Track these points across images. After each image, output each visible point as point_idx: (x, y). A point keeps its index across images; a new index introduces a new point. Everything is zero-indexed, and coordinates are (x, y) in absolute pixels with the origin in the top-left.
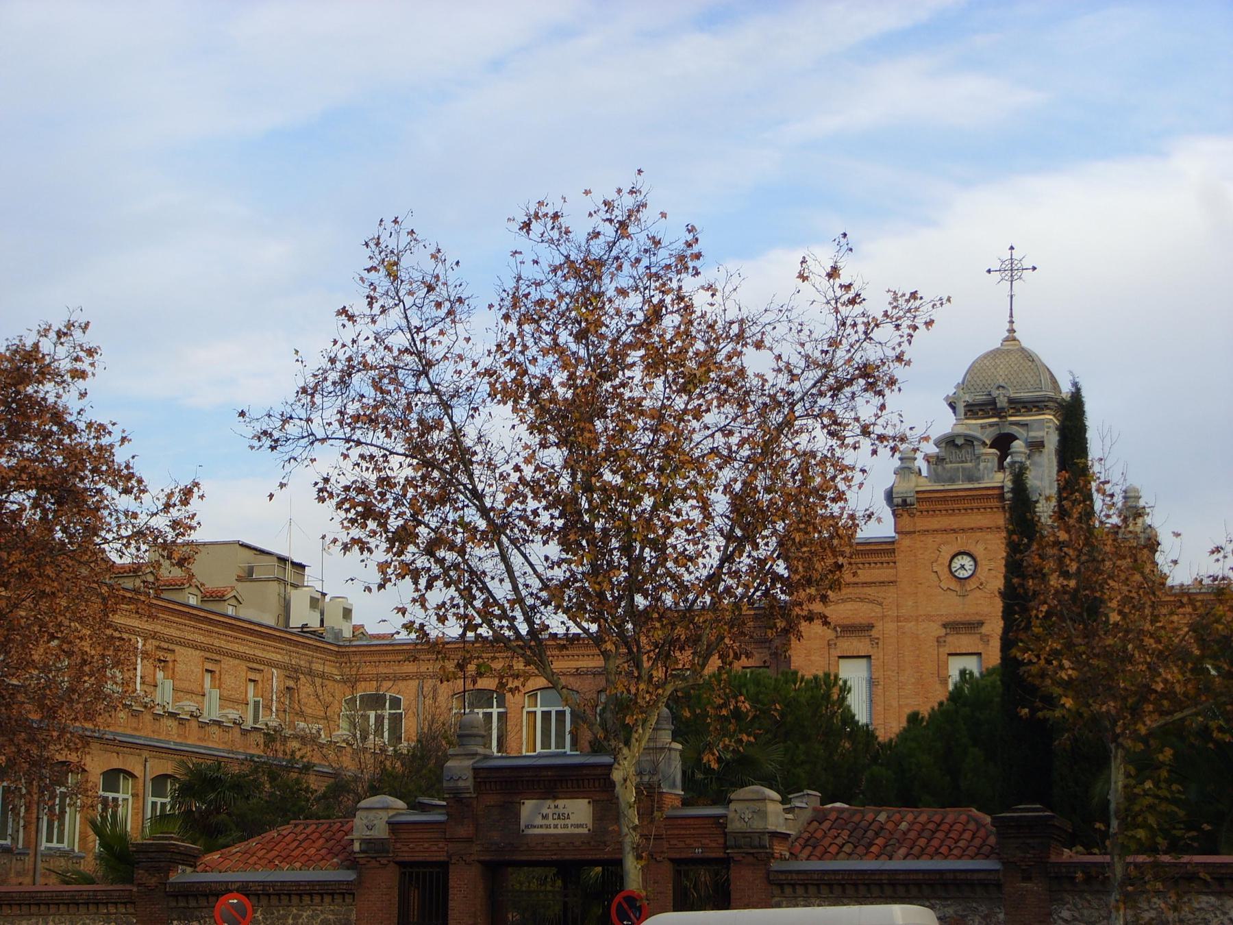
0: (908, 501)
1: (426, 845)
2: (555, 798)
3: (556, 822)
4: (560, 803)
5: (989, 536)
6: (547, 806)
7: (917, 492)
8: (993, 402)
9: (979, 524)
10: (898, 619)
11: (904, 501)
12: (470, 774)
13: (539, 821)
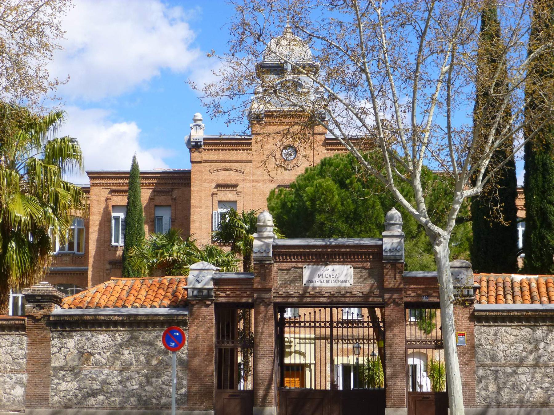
3: (328, 279)
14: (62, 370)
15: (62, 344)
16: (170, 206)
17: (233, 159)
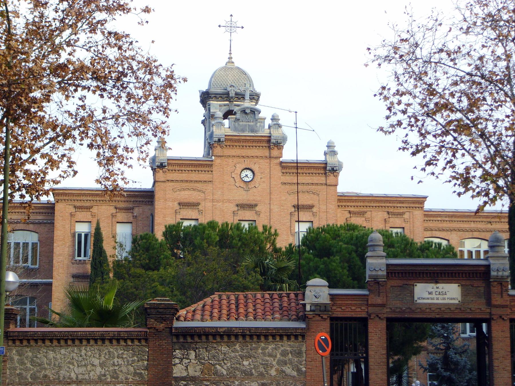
0: (221, 140)
1: (353, 308)
2: (437, 282)
3: (438, 296)
4: (440, 285)
5: (261, 161)
6: (430, 287)
7: (226, 135)
8: (228, 94)
9: (256, 154)
10: (213, 201)
11: (219, 140)
12: (384, 268)
13: (426, 295)
14: (184, 381)
15: (183, 355)
16: (131, 223)
17: (195, 180)
